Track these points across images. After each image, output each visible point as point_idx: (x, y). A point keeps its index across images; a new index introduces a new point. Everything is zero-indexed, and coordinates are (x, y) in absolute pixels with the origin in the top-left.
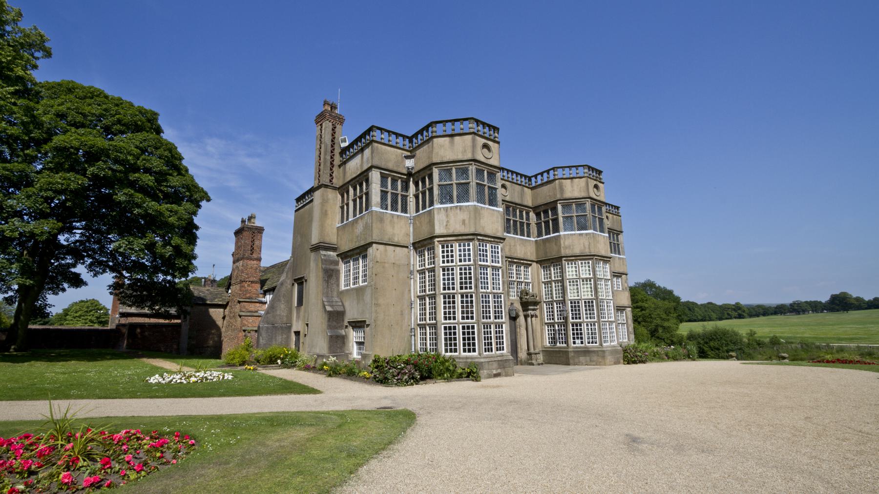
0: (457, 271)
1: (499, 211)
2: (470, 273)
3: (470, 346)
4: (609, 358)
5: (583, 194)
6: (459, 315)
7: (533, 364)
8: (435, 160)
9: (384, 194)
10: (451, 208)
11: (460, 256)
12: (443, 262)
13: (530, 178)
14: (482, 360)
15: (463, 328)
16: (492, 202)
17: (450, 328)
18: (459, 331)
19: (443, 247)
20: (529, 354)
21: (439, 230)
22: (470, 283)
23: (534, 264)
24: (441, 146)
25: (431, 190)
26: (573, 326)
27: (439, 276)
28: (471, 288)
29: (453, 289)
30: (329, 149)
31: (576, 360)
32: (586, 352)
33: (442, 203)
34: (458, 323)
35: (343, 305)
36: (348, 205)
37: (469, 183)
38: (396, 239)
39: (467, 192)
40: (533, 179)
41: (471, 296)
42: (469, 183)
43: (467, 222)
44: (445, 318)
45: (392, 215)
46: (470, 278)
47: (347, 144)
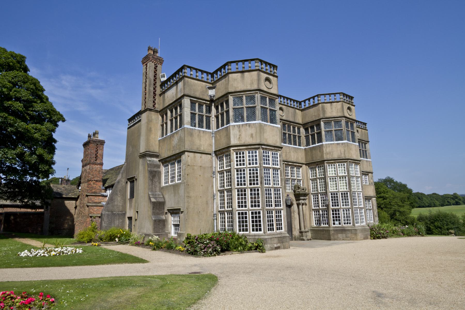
1: (277, 127)
2: (257, 173)
3: (257, 226)
4: (360, 235)
7: (303, 240)
8: (231, 90)
10: (242, 125)
12: (237, 165)
13: (300, 103)
14: (266, 237)
15: (252, 213)
16: (273, 121)
17: (242, 213)
18: (249, 216)
19: (237, 154)
21: (234, 141)
22: (257, 180)
23: (304, 166)
24: (235, 80)
25: (228, 112)
26: (333, 211)
27: (234, 175)
28: (257, 184)
29: (245, 184)
31: (336, 237)
32: (343, 230)
33: (235, 121)
35: (164, 197)
36: (166, 123)
37: (255, 107)
38: (202, 149)
39: (254, 113)
40: (303, 103)
41: (258, 190)
42: (255, 107)
43: (254, 135)
44: (239, 206)
46: (257, 177)
47: (165, 79)
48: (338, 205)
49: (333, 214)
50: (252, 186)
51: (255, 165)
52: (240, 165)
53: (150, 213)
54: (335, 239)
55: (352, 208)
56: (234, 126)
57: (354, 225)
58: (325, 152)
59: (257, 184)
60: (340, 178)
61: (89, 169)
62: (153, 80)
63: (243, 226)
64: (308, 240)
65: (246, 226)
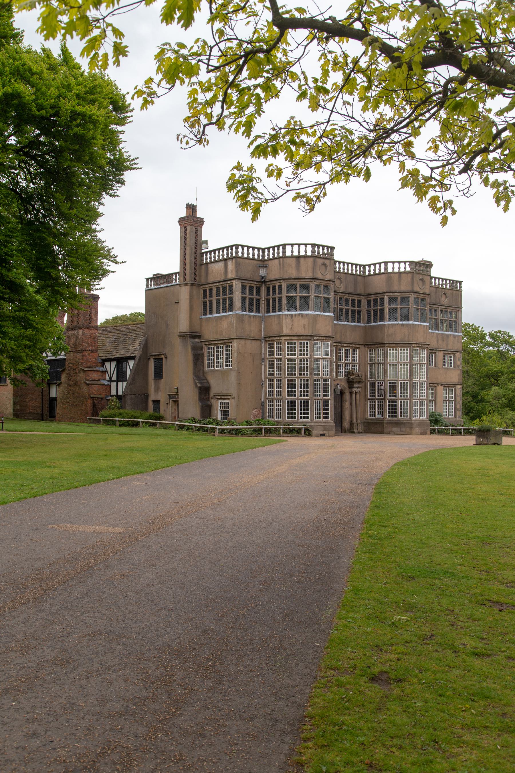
0: (298, 362)
1: (330, 316)
2: (307, 364)
3: (305, 414)
4: (417, 430)
5: (409, 288)
6: (298, 393)
7: (354, 432)
9: (244, 299)
10: (295, 315)
11: (301, 351)
12: (288, 355)
14: (313, 424)
15: (301, 402)
17: (291, 402)
18: (298, 404)
19: (288, 343)
20: (351, 424)
21: (286, 331)
22: (307, 371)
23: (362, 347)
25: (280, 299)
26: (389, 402)
28: (307, 374)
29: (295, 374)
30: (194, 250)
31: (389, 430)
32: (398, 424)
33: (288, 310)
34: (298, 399)
38: (252, 335)
39: (308, 303)
41: (308, 380)
43: (306, 326)
44: (288, 395)
45: (250, 316)
46: (307, 367)
48: (395, 396)
49: (389, 405)
50: (302, 376)
51: (305, 356)
52: (291, 355)
53: (196, 398)
54: (389, 433)
55: (410, 399)
56: (287, 315)
57: (410, 418)
58: (386, 334)
59: (307, 374)
60: (401, 365)
61: (83, 335)
62: (194, 248)
63: (292, 414)
64: (359, 433)
65: (295, 413)
